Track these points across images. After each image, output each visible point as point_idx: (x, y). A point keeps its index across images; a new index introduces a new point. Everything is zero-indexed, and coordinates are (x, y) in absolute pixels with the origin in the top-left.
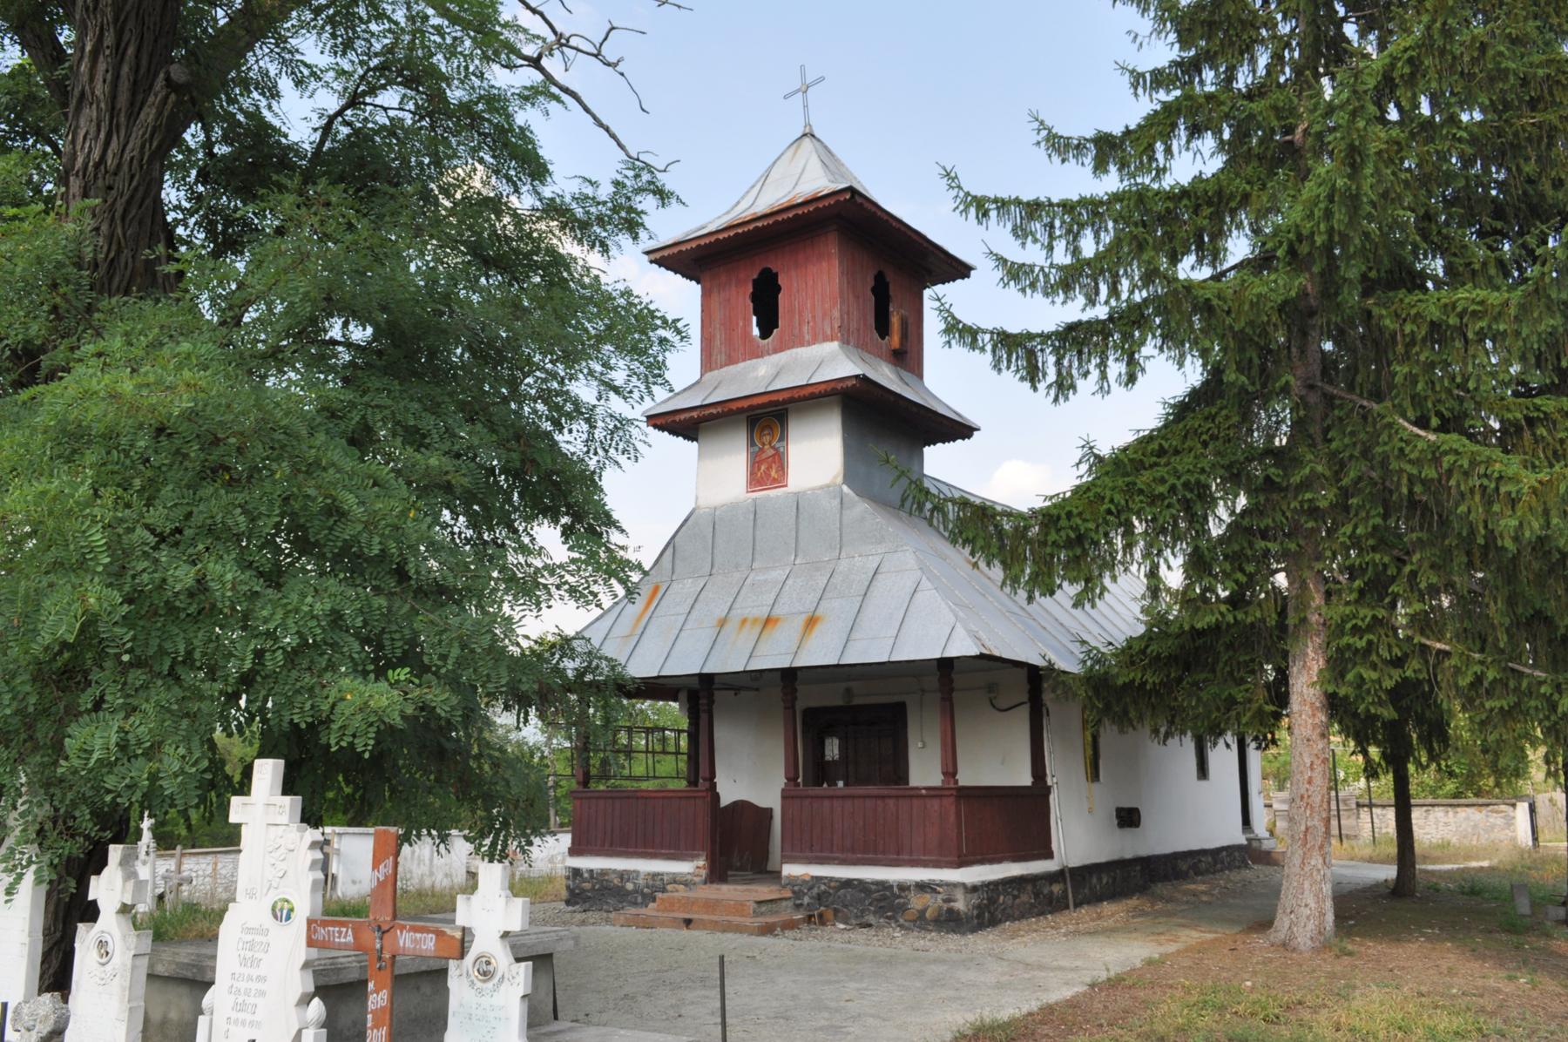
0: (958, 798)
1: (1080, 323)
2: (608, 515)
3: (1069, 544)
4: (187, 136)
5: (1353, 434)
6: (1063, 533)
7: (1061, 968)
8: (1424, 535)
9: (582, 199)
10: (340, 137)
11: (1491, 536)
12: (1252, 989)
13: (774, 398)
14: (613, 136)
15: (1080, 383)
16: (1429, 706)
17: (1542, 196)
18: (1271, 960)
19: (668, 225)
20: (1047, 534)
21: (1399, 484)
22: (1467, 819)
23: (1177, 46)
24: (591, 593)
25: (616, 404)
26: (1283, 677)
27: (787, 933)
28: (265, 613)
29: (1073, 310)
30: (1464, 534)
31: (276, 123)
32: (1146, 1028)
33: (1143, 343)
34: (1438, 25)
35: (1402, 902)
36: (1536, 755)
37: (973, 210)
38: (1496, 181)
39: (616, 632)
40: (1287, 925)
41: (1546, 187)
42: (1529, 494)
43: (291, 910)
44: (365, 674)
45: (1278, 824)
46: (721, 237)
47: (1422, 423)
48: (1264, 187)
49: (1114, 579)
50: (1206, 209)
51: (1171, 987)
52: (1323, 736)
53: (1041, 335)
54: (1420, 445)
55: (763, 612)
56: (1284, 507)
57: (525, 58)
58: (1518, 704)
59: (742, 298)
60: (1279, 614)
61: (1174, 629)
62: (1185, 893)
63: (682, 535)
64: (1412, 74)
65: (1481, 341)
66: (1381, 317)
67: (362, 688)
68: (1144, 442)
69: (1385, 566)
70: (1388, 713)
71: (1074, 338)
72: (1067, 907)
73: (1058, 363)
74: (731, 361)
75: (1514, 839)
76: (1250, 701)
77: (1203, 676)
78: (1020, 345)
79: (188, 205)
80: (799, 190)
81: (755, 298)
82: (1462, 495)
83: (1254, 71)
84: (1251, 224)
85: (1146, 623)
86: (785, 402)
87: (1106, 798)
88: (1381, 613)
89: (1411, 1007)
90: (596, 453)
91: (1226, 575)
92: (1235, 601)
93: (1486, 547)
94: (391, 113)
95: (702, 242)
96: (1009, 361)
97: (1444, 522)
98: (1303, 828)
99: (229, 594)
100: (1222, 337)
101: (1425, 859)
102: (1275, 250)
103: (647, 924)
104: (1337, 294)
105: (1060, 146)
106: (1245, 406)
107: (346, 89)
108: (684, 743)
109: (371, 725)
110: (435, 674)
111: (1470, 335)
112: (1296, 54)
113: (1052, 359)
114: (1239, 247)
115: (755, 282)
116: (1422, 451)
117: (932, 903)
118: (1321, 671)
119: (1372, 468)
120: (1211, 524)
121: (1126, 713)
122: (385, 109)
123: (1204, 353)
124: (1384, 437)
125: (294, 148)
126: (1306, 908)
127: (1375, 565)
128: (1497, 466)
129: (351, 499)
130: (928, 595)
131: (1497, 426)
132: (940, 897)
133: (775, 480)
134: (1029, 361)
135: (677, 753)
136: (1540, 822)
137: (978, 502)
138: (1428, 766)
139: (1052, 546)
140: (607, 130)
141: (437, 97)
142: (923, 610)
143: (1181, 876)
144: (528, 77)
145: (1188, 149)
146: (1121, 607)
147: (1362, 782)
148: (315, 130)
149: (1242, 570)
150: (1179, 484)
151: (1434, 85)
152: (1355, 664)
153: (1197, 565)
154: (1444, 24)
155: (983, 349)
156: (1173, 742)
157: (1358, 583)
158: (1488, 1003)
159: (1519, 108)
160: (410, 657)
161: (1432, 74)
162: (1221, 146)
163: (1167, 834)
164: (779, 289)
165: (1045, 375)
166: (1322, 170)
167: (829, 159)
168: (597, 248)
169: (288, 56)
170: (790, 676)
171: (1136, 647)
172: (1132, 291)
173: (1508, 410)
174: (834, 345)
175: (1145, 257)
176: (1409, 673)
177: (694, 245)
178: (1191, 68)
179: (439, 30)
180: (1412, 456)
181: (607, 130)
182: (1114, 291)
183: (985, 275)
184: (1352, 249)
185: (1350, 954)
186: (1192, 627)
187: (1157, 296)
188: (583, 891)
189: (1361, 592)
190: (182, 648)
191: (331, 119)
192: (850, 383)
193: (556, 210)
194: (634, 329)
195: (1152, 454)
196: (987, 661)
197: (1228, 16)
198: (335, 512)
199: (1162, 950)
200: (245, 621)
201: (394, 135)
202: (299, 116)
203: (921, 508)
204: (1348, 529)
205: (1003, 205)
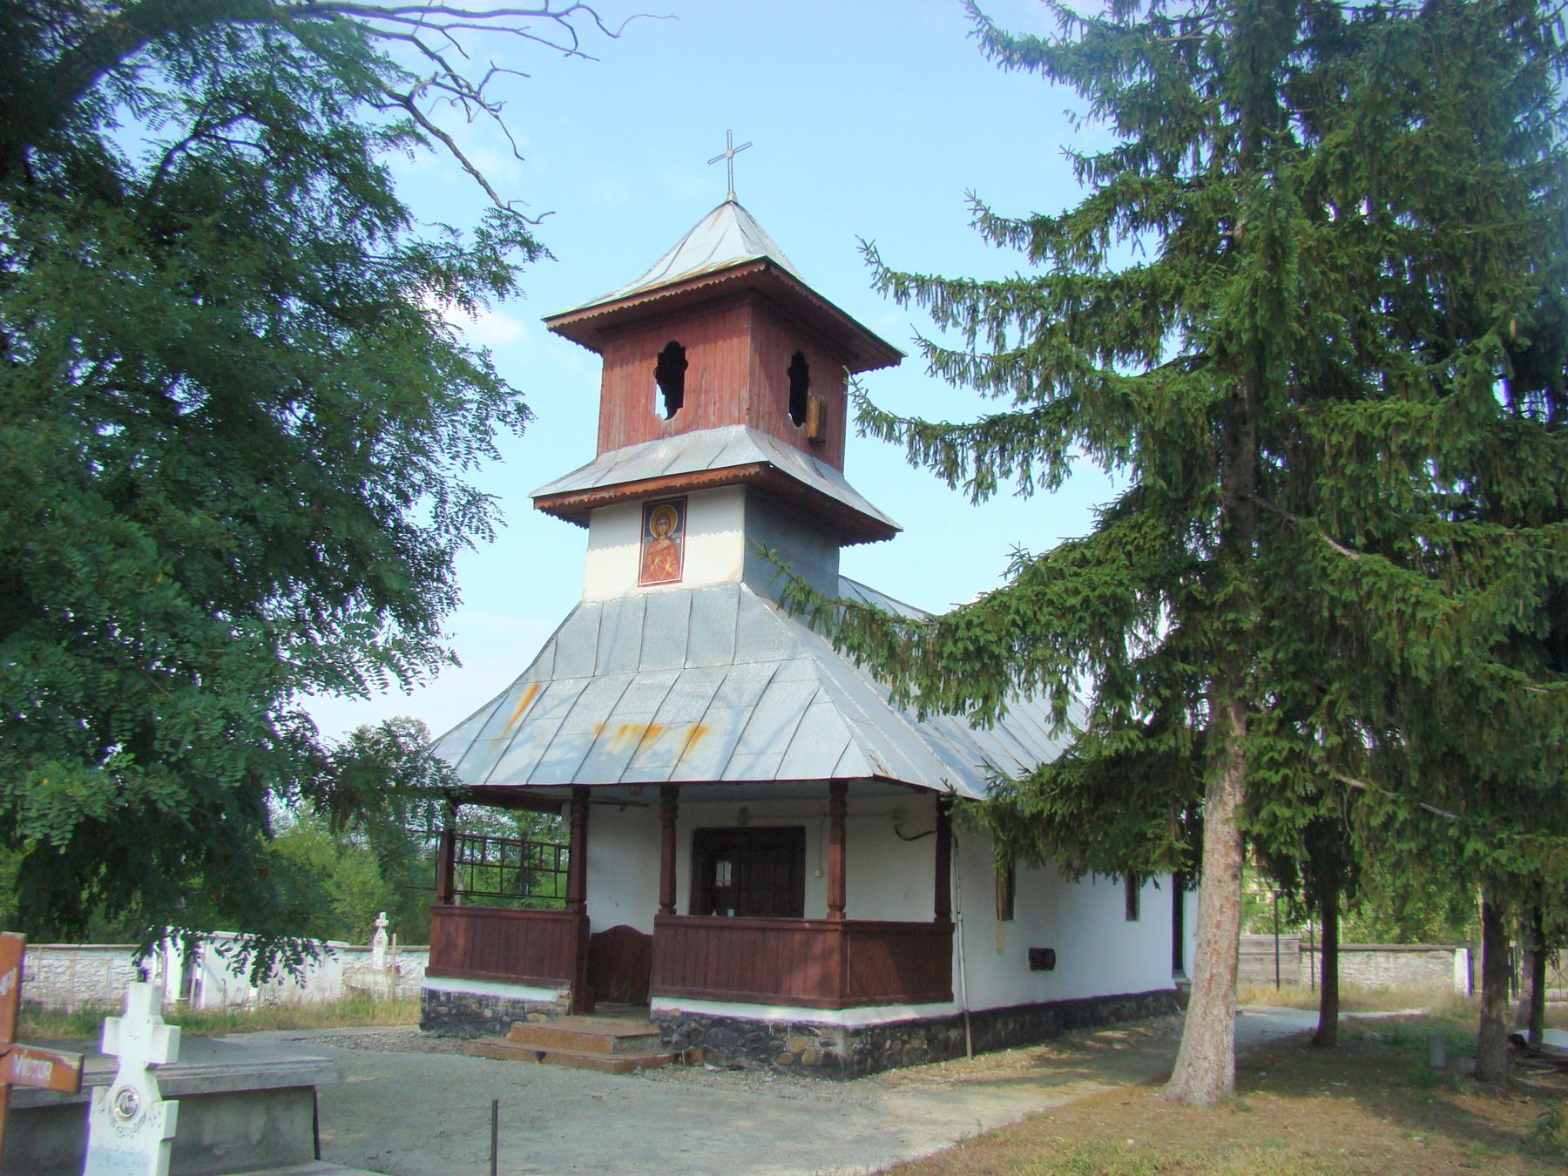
0: (844, 933)
1: (1003, 417)
3: (967, 656)
5: (1279, 549)
7: (933, 1122)
11: (1405, 666)
13: (672, 483)
14: (484, 183)
15: (1001, 483)
18: (1162, 1116)
20: (942, 645)
21: (1321, 608)
22: (1407, 964)
27: (648, 1072)
29: (1004, 403)
30: (1382, 663)
33: (1067, 442)
34: (1367, 120)
35: (1319, 1055)
37: (892, 288)
39: (488, 733)
40: (1184, 1079)
42: (1442, 618)
46: (625, 305)
50: (1137, 308)
52: (1235, 877)
53: (961, 428)
54: (1342, 564)
56: (1206, 627)
58: (1427, 848)
62: (1100, 1039)
63: (539, 624)
64: (1345, 171)
68: (1069, 547)
69: (1304, 694)
71: (998, 434)
72: (965, 1054)
73: (979, 459)
74: (630, 441)
76: (1160, 837)
80: (713, 260)
87: (1018, 938)
90: (447, 531)
95: (605, 311)
96: (926, 455)
97: (1364, 649)
98: (1208, 975)
103: (498, 1055)
105: (997, 229)
108: (565, 856)
111: (1393, 448)
112: (1239, 148)
113: (972, 454)
114: (1172, 346)
115: (662, 358)
116: (1344, 571)
117: (812, 1047)
118: (1236, 807)
124: (1308, 555)
127: (1295, 694)
128: (1415, 590)
129: (77, 557)
130: (825, 709)
132: (817, 1040)
133: (669, 575)
135: (557, 871)
139: (960, 659)
140: (477, 175)
142: (812, 723)
143: (1103, 1023)
146: (1030, 732)
153: (1114, 687)
154: (1374, 120)
164: (685, 364)
165: (964, 471)
167: (750, 225)
170: (670, 792)
173: (1437, 533)
176: (1323, 811)
177: (596, 313)
178: (1136, 156)
180: (1334, 576)
181: (477, 175)
183: (915, 360)
185: (1247, 1110)
188: (439, 1015)
192: (753, 471)
196: (880, 784)
199: (1049, 1103)
205: (922, 283)
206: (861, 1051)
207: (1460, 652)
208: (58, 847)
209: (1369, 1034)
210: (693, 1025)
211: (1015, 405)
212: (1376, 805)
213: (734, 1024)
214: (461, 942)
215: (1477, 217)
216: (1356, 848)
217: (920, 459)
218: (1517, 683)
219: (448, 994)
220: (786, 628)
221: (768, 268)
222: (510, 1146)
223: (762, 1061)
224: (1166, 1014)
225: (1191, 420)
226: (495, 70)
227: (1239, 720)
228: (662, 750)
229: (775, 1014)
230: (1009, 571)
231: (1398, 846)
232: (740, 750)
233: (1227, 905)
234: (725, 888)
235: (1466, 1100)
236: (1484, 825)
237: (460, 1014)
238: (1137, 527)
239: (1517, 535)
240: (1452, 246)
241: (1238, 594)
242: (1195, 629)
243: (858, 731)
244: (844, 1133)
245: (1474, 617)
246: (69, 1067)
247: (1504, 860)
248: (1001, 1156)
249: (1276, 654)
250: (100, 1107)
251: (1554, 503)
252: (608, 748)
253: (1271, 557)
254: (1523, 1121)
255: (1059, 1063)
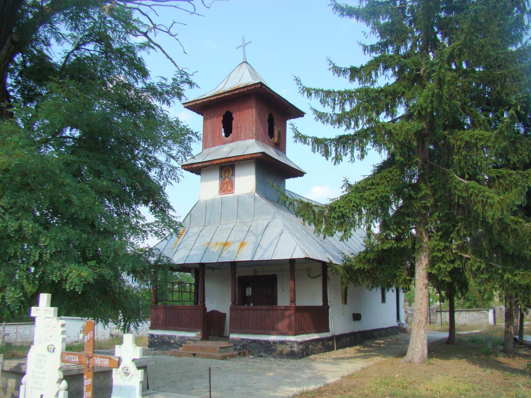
1: (344, 136)
2: (169, 204)
3: (339, 218)
4: (16, 59)
5: (439, 180)
6: (337, 214)
8: (462, 217)
9: (162, 85)
10: (72, 60)
11: (484, 217)
12: (398, 377)
13: (230, 160)
14: (173, 62)
16: (462, 277)
17: (502, 98)
18: (405, 367)
19: (192, 94)
20: (331, 214)
21: (454, 199)
22: (473, 316)
23: (379, 38)
24: (163, 234)
25: (173, 162)
26: (413, 267)
28: (43, 239)
29: (341, 131)
31: (48, 54)
32: (361, 392)
33: (367, 144)
34: (468, 38)
36: (496, 293)
37: (306, 93)
38: (487, 92)
40: (411, 354)
41: (503, 95)
42: (496, 202)
43: (54, 349)
44: (79, 263)
45: (409, 318)
47: (462, 176)
48: (410, 90)
49: (355, 230)
50: (387, 98)
51: (370, 377)
52: (426, 288)
54: (462, 185)
55: (224, 240)
56: (415, 205)
57: (141, 32)
58: (491, 277)
59: (218, 121)
60: (412, 244)
61: (375, 249)
63: (201, 213)
64: (460, 54)
65: (482, 149)
66: (450, 139)
67: (78, 268)
69: (449, 227)
70: (448, 279)
71: (343, 141)
72: (334, 349)
73: (336, 150)
74: (214, 145)
75: (488, 322)
76: (401, 275)
77: (386, 266)
78: (322, 143)
79: (14, 84)
81: (224, 122)
82: (475, 203)
83: (406, 48)
84: (405, 103)
85: (365, 246)
86: (234, 161)
87: (349, 310)
88: (447, 244)
89: (451, 382)
90: (163, 179)
91: (395, 230)
92: (398, 239)
93: (482, 221)
94: (92, 52)
96: (318, 149)
97: (469, 212)
98: (418, 320)
99: (31, 232)
100: (395, 144)
101: (459, 330)
102: (414, 112)
103: (179, 355)
104: (435, 129)
105: (338, 70)
106: (402, 167)
107: (74, 42)
108: (193, 288)
109: (82, 281)
110: (105, 263)
111: (479, 147)
112: (421, 44)
113: (334, 149)
114: (401, 111)
115: (224, 116)
117: (287, 349)
118: (426, 265)
119: (446, 192)
120: (390, 211)
121: (357, 279)
122: (89, 50)
123: (388, 149)
124: (450, 181)
125: (55, 64)
126: (418, 346)
127: (446, 227)
128: (487, 193)
130: (286, 235)
131: (487, 178)
132: (288, 346)
133: (230, 191)
134: (325, 149)
136: (497, 316)
137: (306, 201)
138: (461, 298)
139: (333, 218)
141: (109, 46)
142: (283, 240)
143: (376, 338)
144: (142, 39)
145: (383, 74)
147: (438, 303)
148: (63, 58)
149: (400, 228)
150: (379, 196)
151: (467, 58)
152: (438, 262)
153: (384, 226)
154: (470, 38)
155: (308, 144)
156: (374, 290)
157: (440, 233)
158: (477, 379)
159: (495, 68)
160: (96, 257)
161: (466, 54)
162: (395, 73)
163: (370, 323)
164: (233, 119)
165: (331, 154)
166: (430, 86)
167: (252, 71)
168: (166, 103)
169: (54, 31)
170: (234, 264)
171: (362, 255)
172: (362, 125)
173: (491, 173)
174: (253, 141)
175: (368, 114)
176: (456, 266)
177: (201, 101)
178: (383, 46)
179: (110, 22)
180: (459, 189)
181: (171, 60)
182: (357, 124)
183: (310, 116)
184: (440, 114)
185: (432, 364)
186: (382, 248)
187: (372, 127)
188: (155, 342)
189: (441, 236)
190: (13, 251)
191: (69, 54)
193: (151, 89)
194: (179, 135)
195: (369, 185)
196: (307, 260)
197: (397, 29)
198: (68, 202)
199: (367, 364)
200: (36, 243)
201: (92, 60)
202: (57, 52)
203: (285, 202)
204: (437, 214)
205: (317, 91)
206: (302, 349)
207: (503, 213)
208: (78, 292)
209: (464, 339)
210: (245, 343)
211: (345, 131)
212: (473, 262)
213: (259, 342)
214: (162, 316)
215: (502, 67)
216: (467, 277)
217: (316, 150)
218: (521, 223)
219: (158, 335)
220: (271, 208)
221: (261, 86)
222: (197, 384)
223: (269, 354)
224: (395, 334)
225: (410, 137)
226: (175, 23)
227: (426, 236)
228: (231, 250)
229: (273, 338)
230: (343, 186)
231: (482, 276)
232: (259, 249)
233: (424, 297)
234: (250, 296)
235: (502, 359)
236: (510, 269)
237: (163, 342)
238: (390, 172)
239: (517, 173)
240: (494, 77)
241: (426, 194)
242: (412, 206)
243: (298, 242)
244: (305, 376)
245: (507, 202)
246: (115, 360)
247: (517, 280)
248: (357, 381)
249: (439, 213)
250: (116, 373)
251: (528, 162)
252: (212, 249)
253: (437, 182)
254: (520, 365)
255: (365, 352)
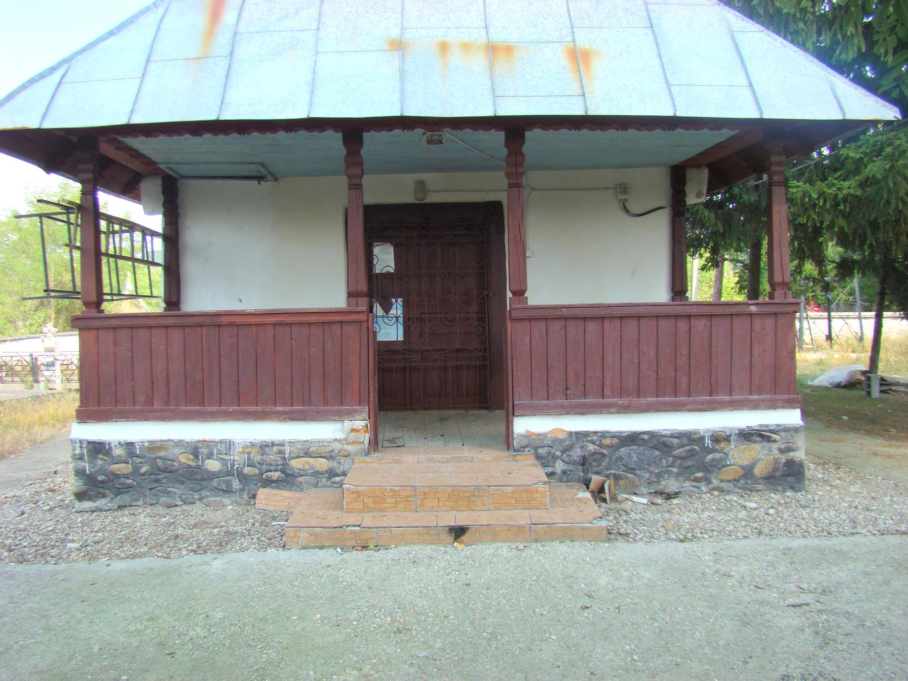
117: (762, 457)
132: (774, 446)
210: (591, 447)
213: (658, 442)
219: (129, 445)
223: (697, 480)
